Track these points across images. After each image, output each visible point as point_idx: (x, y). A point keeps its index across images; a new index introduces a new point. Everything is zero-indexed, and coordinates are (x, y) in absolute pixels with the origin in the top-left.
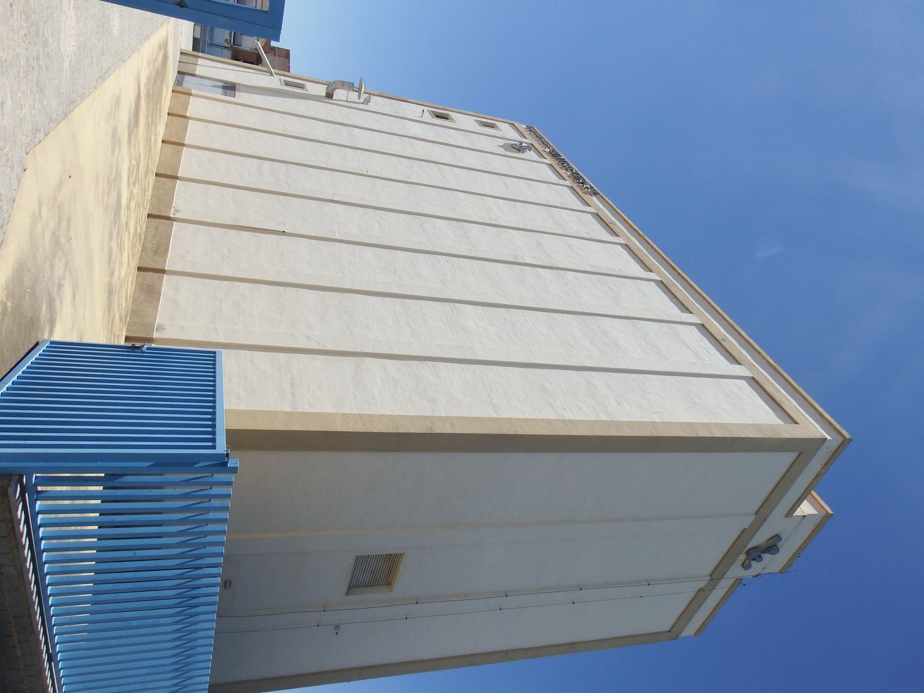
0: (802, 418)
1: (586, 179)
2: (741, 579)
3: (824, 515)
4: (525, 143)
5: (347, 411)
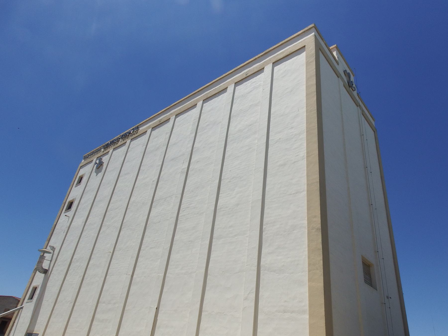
0: (301, 44)
4: (96, 161)
5: (306, 278)
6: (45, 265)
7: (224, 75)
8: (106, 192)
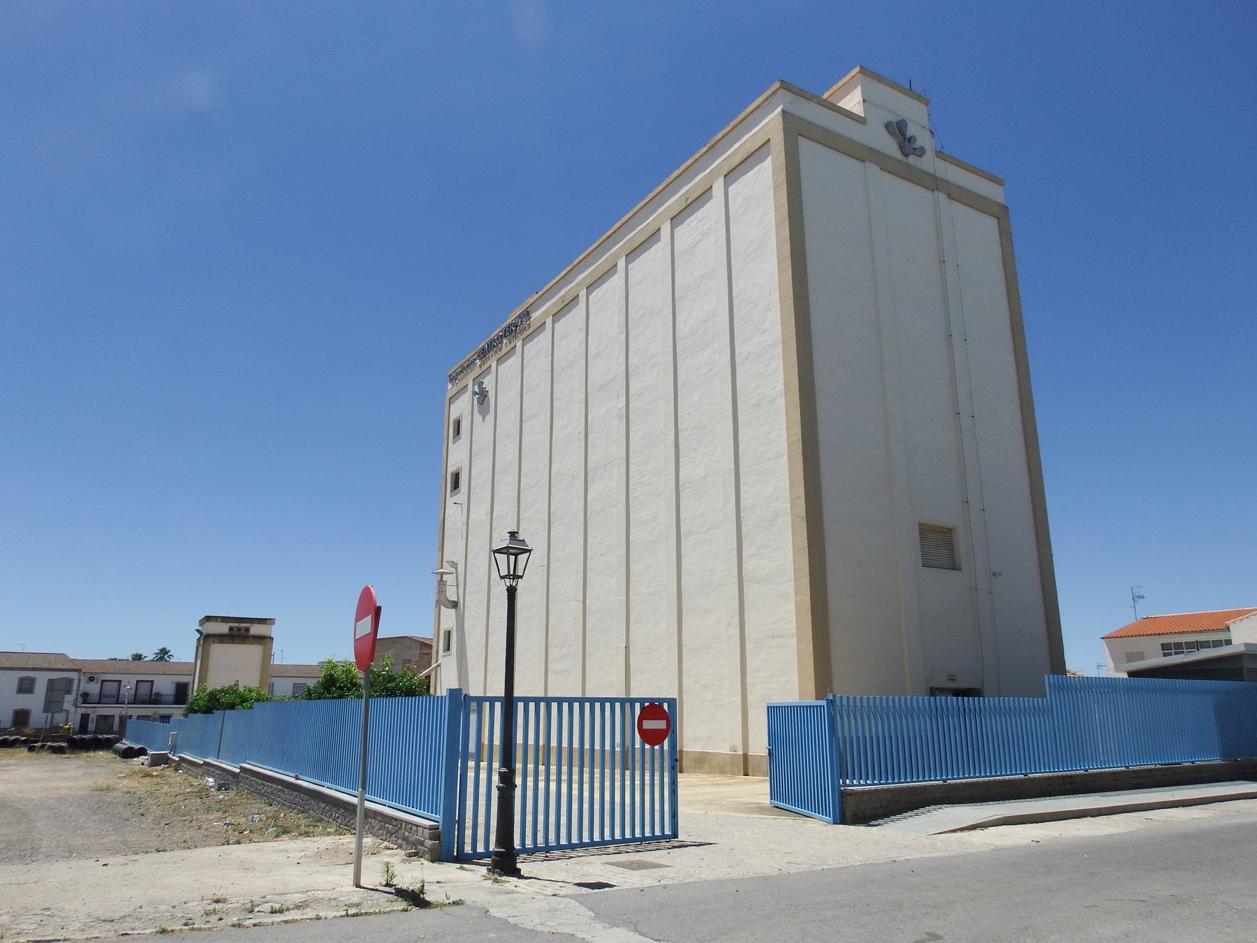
0: (763, 133)
1: (509, 321)
2: (936, 151)
3: (862, 75)
4: (473, 388)
5: (792, 591)
6: (451, 595)
7: (651, 196)
8: (507, 454)
